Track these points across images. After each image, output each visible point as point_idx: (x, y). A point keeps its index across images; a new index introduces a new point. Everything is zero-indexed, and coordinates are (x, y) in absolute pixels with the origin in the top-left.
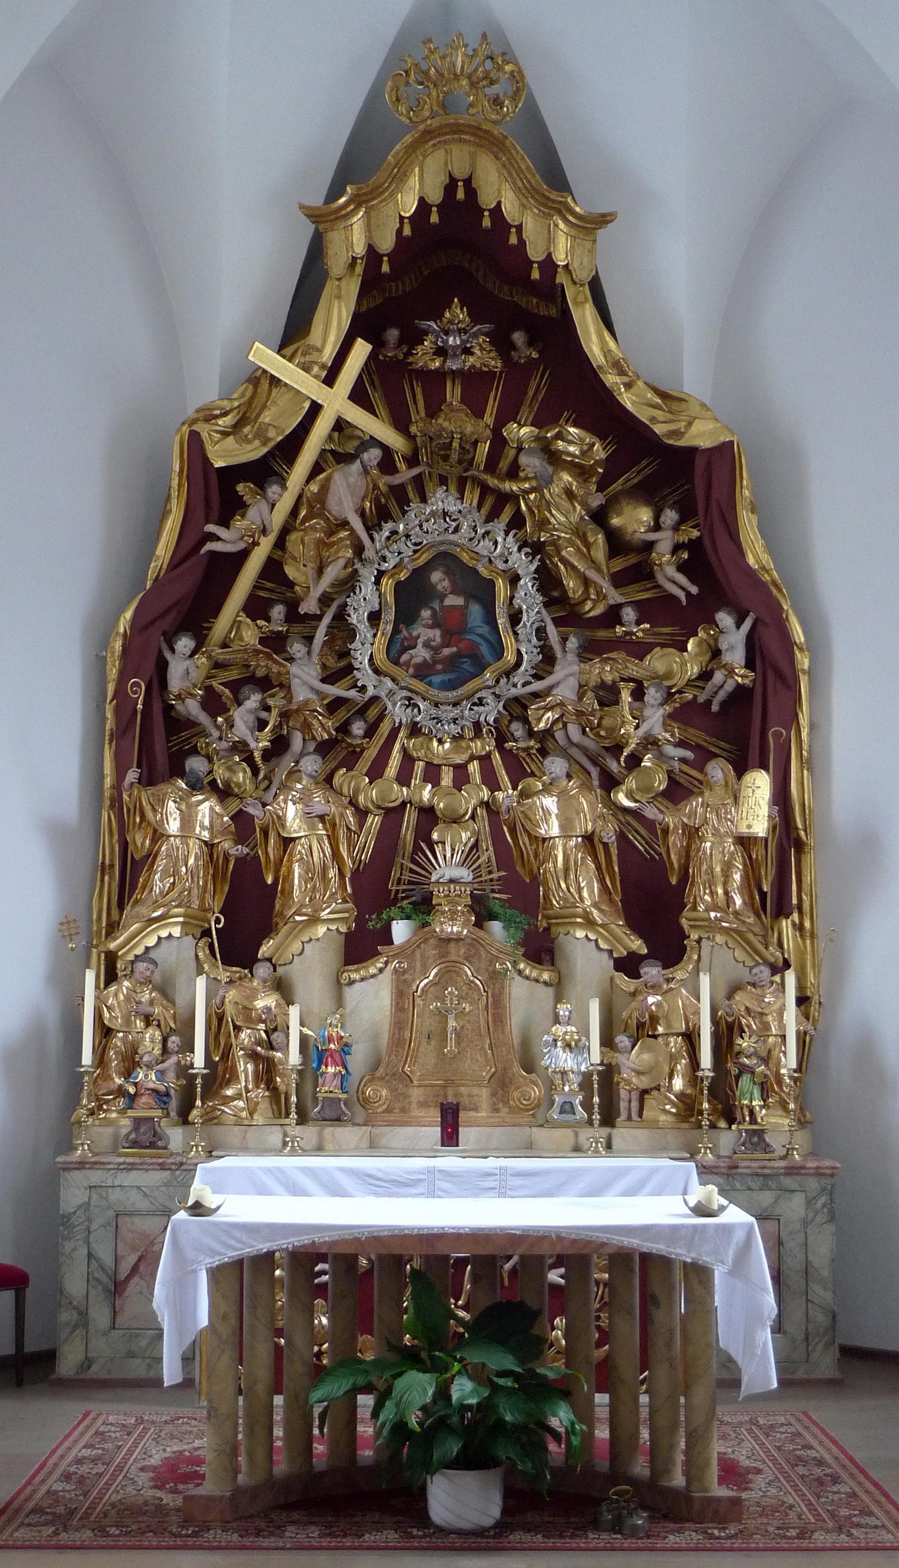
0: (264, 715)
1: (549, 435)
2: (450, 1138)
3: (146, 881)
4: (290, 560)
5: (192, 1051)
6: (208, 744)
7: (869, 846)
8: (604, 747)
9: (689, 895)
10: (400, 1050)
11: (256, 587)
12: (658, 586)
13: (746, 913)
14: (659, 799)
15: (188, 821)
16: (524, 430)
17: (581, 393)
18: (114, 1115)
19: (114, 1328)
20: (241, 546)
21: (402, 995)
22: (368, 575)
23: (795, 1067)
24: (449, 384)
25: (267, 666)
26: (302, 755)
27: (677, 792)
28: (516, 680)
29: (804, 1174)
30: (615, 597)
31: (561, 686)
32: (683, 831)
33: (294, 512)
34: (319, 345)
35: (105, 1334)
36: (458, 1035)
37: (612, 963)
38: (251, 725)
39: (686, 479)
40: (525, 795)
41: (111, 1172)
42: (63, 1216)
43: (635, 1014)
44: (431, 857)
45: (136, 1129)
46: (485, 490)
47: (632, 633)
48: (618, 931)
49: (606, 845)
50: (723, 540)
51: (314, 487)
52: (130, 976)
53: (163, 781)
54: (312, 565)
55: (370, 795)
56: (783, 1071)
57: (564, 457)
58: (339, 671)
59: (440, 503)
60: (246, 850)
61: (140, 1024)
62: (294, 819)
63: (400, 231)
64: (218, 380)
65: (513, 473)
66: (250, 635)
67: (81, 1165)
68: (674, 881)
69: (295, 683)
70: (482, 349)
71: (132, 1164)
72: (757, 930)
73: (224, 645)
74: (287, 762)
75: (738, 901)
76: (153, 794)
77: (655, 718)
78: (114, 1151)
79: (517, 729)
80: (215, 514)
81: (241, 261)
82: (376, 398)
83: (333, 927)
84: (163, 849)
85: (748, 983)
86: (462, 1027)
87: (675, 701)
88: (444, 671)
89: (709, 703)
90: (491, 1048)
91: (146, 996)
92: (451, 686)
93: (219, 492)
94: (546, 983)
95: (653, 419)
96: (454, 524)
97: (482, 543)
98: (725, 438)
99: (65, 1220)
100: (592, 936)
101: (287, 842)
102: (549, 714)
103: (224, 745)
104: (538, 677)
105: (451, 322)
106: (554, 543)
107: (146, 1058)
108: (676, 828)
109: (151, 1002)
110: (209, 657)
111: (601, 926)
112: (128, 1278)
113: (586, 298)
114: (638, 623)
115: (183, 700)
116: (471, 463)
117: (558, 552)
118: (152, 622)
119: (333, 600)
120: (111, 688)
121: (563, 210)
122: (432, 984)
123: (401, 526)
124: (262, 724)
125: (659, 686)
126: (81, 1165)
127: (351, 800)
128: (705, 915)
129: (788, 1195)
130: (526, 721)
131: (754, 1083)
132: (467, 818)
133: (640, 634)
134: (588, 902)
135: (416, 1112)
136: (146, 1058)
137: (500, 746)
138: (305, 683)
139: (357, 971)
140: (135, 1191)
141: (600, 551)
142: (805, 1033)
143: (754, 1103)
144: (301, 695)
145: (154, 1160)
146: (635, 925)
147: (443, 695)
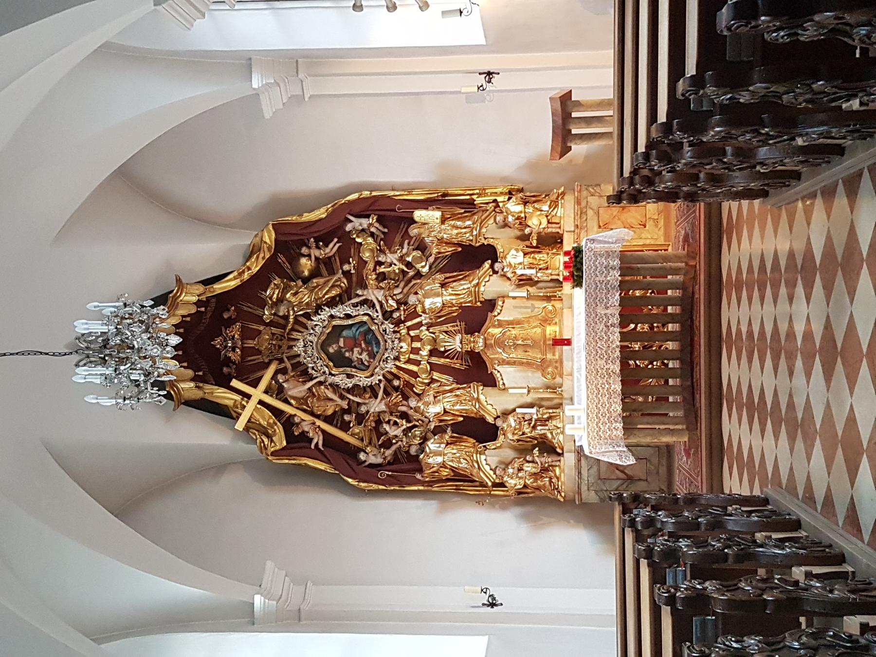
0: (392, 422)
2: (568, 342)
11: (336, 426)
12: (334, 255)
15: (439, 454)
16: (266, 313)
20: (320, 433)
22: (331, 379)
26: (409, 406)
27: (422, 247)
30: (340, 275)
39: (290, 241)
40: (424, 312)
46: (293, 329)
50: (314, 229)
51: (293, 402)
55: (424, 378)
63: (184, 367)
65: (286, 317)
68: (460, 249)
69: (377, 410)
72: (480, 214)
73: (362, 440)
74: (411, 412)
75: (468, 223)
77: (391, 257)
79: (396, 315)
80: (307, 444)
81: (200, 434)
91: (510, 471)
92: (378, 343)
95: (263, 258)
100: (483, 283)
103: (404, 439)
104: (374, 306)
114: (350, 263)
120: (381, 487)
121: (176, 298)
124: (396, 423)
125: (378, 256)
130: (392, 312)
134: (469, 285)
137: (403, 322)
144: (383, 407)
146: (479, 266)
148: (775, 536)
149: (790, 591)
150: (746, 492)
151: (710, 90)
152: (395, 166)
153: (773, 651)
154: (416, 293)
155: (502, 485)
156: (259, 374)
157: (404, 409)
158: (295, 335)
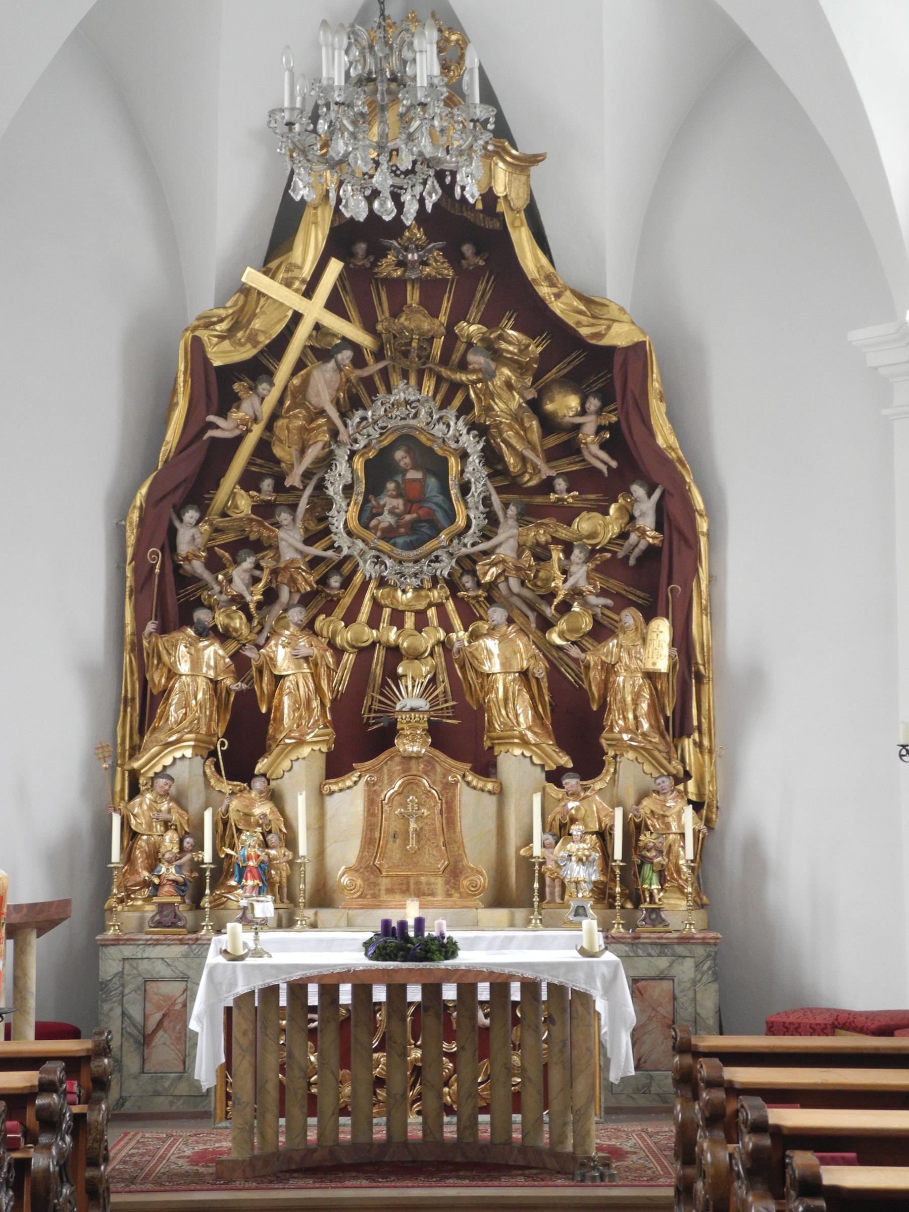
0: (257, 573)
1: (492, 336)
3: (163, 712)
4: (277, 443)
5: (203, 850)
6: (210, 596)
7: (756, 678)
8: (540, 596)
9: (607, 720)
10: (371, 847)
11: (250, 463)
12: (584, 460)
13: (652, 734)
14: (586, 638)
15: (195, 664)
16: (473, 328)
17: (518, 299)
18: (140, 903)
19: (143, 1072)
20: (237, 433)
21: (372, 802)
22: (342, 455)
23: (692, 858)
24: (409, 288)
25: (258, 531)
27: (601, 631)
28: (466, 540)
29: (693, 944)
30: (546, 472)
31: (503, 546)
32: (602, 668)
33: (281, 401)
35: (136, 1078)
36: (418, 835)
37: (544, 775)
38: (247, 581)
39: (609, 373)
40: (475, 636)
41: (141, 947)
42: (102, 983)
43: (558, 817)
44: (395, 690)
45: (160, 912)
47: (563, 500)
48: (549, 750)
49: (537, 679)
51: (296, 381)
53: (175, 630)
54: (295, 447)
55: (345, 637)
56: (681, 862)
57: (505, 354)
58: (318, 533)
59: (402, 394)
60: (244, 686)
61: (159, 828)
62: (284, 660)
64: (213, 291)
65: (463, 366)
66: (244, 503)
67: (116, 942)
68: (595, 708)
69: (282, 545)
70: (436, 261)
71: (157, 940)
72: (661, 747)
73: (224, 515)
74: (277, 610)
76: (167, 640)
77: (579, 573)
78: (141, 930)
79: (467, 581)
81: (232, 197)
82: (348, 302)
83: (316, 748)
84: (177, 685)
85: (654, 791)
86: (421, 829)
87: (596, 559)
88: (406, 534)
89: (627, 557)
90: (445, 845)
92: (412, 546)
93: (219, 388)
94: (490, 792)
95: (579, 323)
96: (414, 411)
97: (437, 427)
98: (638, 338)
99: (104, 986)
100: (527, 754)
101: (278, 679)
102: (494, 569)
103: (224, 597)
104: (486, 537)
105: (409, 239)
106: (498, 426)
107: (167, 856)
108: (596, 664)
109: (169, 811)
110: (211, 525)
111: (534, 745)
112: (155, 1031)
113: (521, 221)
114: (569, 491)
115: (190, 561)
116: (428, 358)
117: (501, 435)
119: (314, 474)
120: (130, 551)
122: (398, 793)
123: (370, 413)
124: (256, 580)
125: (583, 547)
126: (116, 942)
127: (329, 641)
128: (618, 736)
129: (680, 960)
130: (474, 573)
131: (653, 871)
132: (426, 655)
133: (570, 500)
134: (524, 726)
136: (167, 856)
138: (290, 545)
139: (336, 783)
140: (160, 961)
142: (699, 831)
143: (653, 887)
144: (288, 555)
145: (175, 937)
146: (562, 744)
147: (406, 554)
154: (510, 621)
155: (135, 790)
156: (353, 313)
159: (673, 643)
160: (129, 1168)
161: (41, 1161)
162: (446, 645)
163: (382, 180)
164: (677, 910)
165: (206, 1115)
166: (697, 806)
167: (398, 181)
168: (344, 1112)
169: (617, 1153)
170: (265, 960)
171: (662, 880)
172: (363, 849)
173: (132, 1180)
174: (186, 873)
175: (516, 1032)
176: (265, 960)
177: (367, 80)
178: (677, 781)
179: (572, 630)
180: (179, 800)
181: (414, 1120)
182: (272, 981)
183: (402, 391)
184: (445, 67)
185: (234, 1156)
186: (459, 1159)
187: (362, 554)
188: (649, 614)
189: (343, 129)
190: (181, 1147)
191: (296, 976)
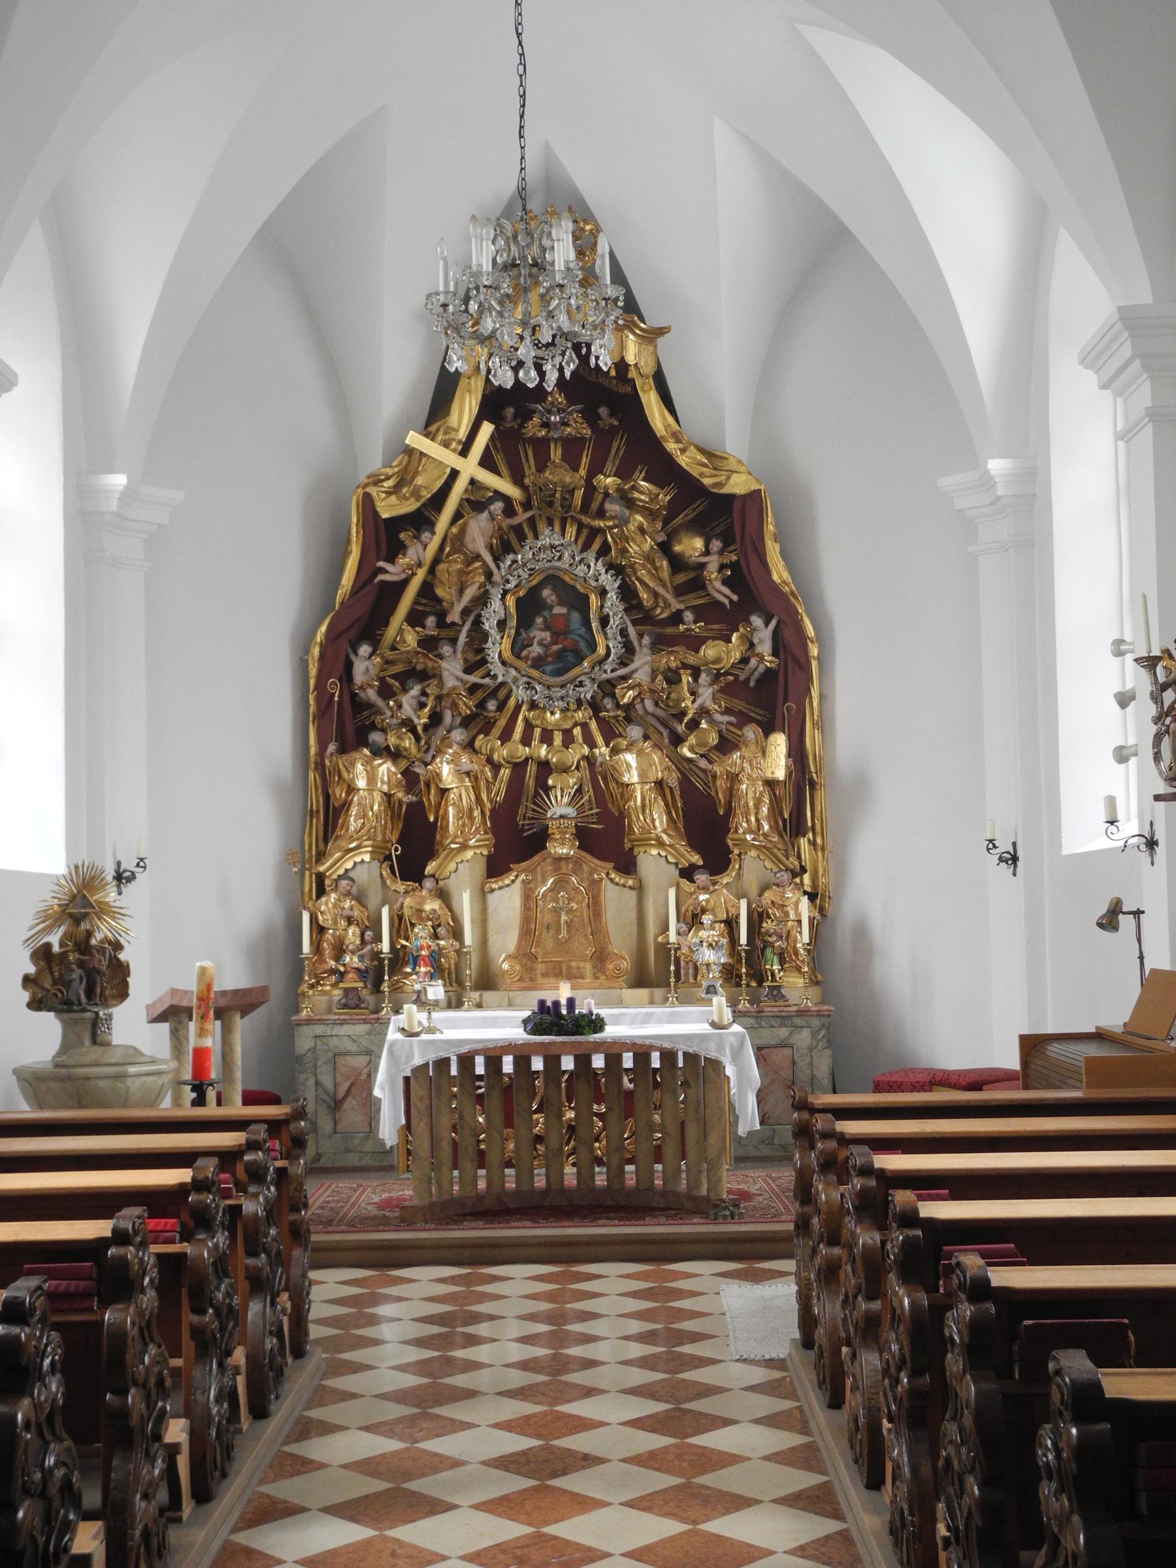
0: (423, 699)
6: (383, 720)
7: (862, 784)
11: (416, 602)
12: (709, 595)
15: (371, 779)
16: (609, 480)
20: (403, 576)
21: (528, 897)
22: (496, 594)
24: (552, 446)
27: (726, 745)
30: (676, 605)
34: (456, 426)
35: (329, 1137)
40: (615, 751)
43: (691, 908)
48: (682, 849)
49: (671, 788)
50: (753, 559)
51: (454, 530)
52: (336, 889)
55: (502, 753)
58: (476, 663)
61: (343, 923)
65: (601, 514)
66: (411, 638)
67: (309, 1022)
69: (445, 674)
70: (576, 422)
73: (393, 648)
74: (442, 731)
77: (706, 695)
78: (329, 1011)
79: (608, 703)
80: (384, 553)
81: (396, 371)
82: (499, 459)
83: (478, 851)
88: (554, 662)
89: (748, 680)
91: (347, 904)
93: (386, 537)
94: (631, 888)
95: (702, 475)
98: (754, 486)
99: (299, 1059)
100: (663, 854)
101: (444, 792)
102: (631, 692)
103: (395, 721)
104: (623, 664)
105: (552, 403)
107: (351, 947)
108: (722, 774)
109: (351, 908)
110: (382, 657)
114: (695, 622)
116: (570, 506)
117: (635, 573)
118: (340, 635)
119: (472, 611)
120: (312, 682)
122: (551, 890)
124: (422, 705)
125: (709, 671)
126: (309, 1022)
130: (613, 696)
135: (540, 980)
136: (351, 947)
138: (452, 674)
139: (496, 882)
141: (665, 573)
144: (450, 682)
146: (693, 845)
148: (241, 1381)
149: (144, 1432)
150: (317, 1310)
151: (966, 1310)
152: (861, 700)
153: (39, 1427)
154: (646, 737)
155: (321, 891)
156: (503, 469)
157: (448, 717)
158: (571, 531)
159: (789, 755)
160: (326, 1213)
161: (251, 1207)
162: (590, 760)
163: (526, 352)
164: (796, 987)
165: (390, 1168)
166: (812, 897)
167: (540, 353)
168: (509, 1164)
169: (746, 1196)
170: (437, 1036)
171: (782, 962)
172: (520, 939)
173: (329, 1222)
174: (367, 962)
175: (657, 1095)
176: (437, 1036)
177: (511, 266)
178: (794, 874)
179: (699, 745)
180: (360, 899)
181: (569, 1170)
182: (444, 1054)
183: (548, 537)
184: (580, 253)
185: (416, 1202)
186: (609, 1203)
187: (515, 680)
188: (768, 729)
189: (491, 309)
190: (370, 1194)
191: (464, 1050)
